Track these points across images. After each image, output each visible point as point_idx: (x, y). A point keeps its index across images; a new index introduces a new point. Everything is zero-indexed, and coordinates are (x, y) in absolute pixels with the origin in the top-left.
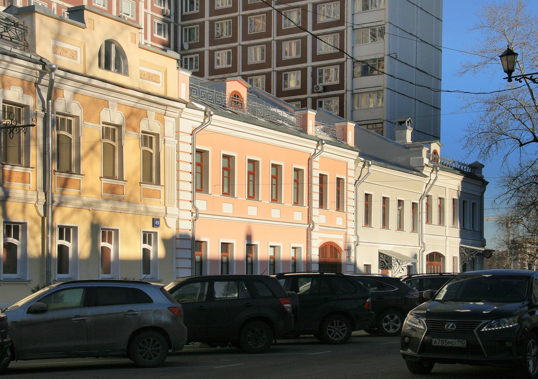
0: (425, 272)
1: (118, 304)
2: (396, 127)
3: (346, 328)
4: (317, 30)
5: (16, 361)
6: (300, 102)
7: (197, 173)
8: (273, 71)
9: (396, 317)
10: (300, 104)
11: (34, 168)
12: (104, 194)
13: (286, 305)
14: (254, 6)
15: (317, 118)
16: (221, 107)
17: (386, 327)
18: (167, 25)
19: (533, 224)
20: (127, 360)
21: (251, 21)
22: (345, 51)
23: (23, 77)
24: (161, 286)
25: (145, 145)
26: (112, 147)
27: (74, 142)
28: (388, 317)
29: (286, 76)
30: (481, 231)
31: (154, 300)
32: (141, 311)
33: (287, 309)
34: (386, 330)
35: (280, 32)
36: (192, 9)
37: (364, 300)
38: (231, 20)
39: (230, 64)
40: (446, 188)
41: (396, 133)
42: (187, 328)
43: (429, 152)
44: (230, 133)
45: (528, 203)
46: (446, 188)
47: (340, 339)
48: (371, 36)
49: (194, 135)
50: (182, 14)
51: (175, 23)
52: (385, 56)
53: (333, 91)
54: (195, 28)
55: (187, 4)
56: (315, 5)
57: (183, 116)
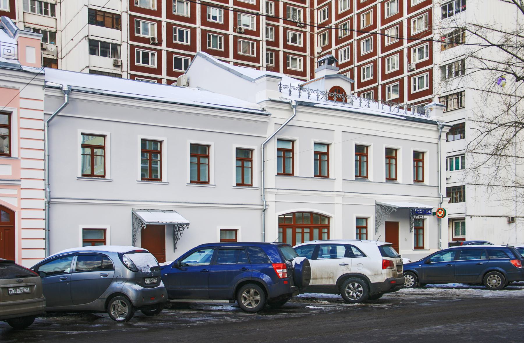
0: (153, 149)
1: (211, 62)
2: (398, 273)
3: (126, 314)
4: (223, 30)
5: (450, 202)
6: (399, 82)
7: (7, 123)
8: (355, 67)
9: (258, 297)
10: (154, 66)
11: (42, 100)
12: (460, 233)
13: (278, 271)
14: (365, 4)
15: (153, 144)
16: (461, 35)
17: (247, 306)
18: (274, 3)
19: (361, 295)
20: (336, 296)
21: (264, 211)
22: (200, 5)
23: (451, 226)
24: (130, 17)
25: (448, 35)
26: (50, 123)
27: (489, 262)
28: (258, 297)
29: (103, 244)
30: (111, 16)
31: (386, 278)
32: (252, 277)
33: (279, 274)
34: (500, 285)
35: (410, 39)
36: (324, 18)
37: (29, 288)
38: (349, 46)
39: (427, 57)
40: (4, 55)
41: (34, 1)
42: (8, 323)
43: (15, 288)
44: (465, 286)
45: (170, 324)
46: (4, 55)
47: (251, 307)
48: (338, 60)
49: (330, 305)
50: (154, 69)
51: (311, 32)
52: (198, 56)
53: (424, 67)
54: (423, 76)
55: (294, 5)
56: (382, 4)
57: (41, 145)
